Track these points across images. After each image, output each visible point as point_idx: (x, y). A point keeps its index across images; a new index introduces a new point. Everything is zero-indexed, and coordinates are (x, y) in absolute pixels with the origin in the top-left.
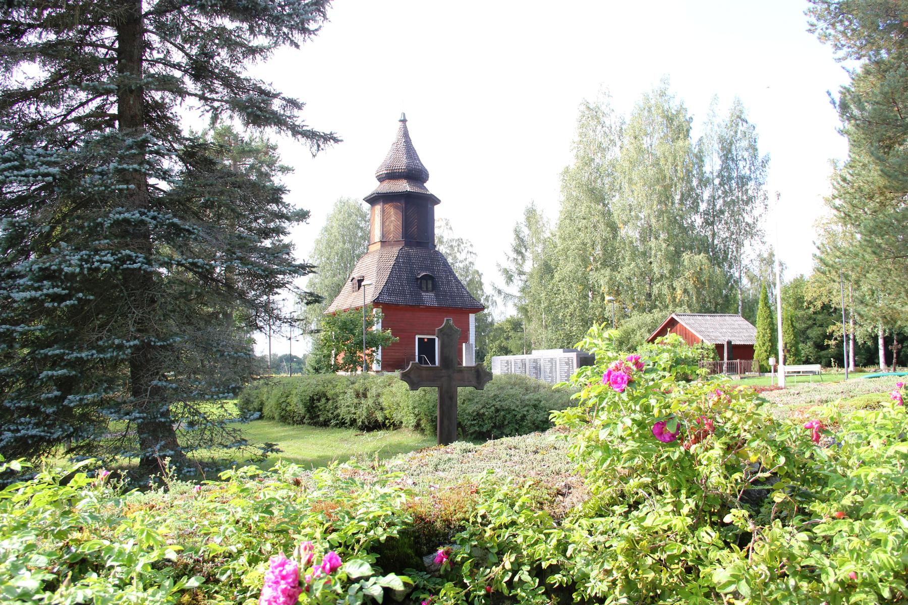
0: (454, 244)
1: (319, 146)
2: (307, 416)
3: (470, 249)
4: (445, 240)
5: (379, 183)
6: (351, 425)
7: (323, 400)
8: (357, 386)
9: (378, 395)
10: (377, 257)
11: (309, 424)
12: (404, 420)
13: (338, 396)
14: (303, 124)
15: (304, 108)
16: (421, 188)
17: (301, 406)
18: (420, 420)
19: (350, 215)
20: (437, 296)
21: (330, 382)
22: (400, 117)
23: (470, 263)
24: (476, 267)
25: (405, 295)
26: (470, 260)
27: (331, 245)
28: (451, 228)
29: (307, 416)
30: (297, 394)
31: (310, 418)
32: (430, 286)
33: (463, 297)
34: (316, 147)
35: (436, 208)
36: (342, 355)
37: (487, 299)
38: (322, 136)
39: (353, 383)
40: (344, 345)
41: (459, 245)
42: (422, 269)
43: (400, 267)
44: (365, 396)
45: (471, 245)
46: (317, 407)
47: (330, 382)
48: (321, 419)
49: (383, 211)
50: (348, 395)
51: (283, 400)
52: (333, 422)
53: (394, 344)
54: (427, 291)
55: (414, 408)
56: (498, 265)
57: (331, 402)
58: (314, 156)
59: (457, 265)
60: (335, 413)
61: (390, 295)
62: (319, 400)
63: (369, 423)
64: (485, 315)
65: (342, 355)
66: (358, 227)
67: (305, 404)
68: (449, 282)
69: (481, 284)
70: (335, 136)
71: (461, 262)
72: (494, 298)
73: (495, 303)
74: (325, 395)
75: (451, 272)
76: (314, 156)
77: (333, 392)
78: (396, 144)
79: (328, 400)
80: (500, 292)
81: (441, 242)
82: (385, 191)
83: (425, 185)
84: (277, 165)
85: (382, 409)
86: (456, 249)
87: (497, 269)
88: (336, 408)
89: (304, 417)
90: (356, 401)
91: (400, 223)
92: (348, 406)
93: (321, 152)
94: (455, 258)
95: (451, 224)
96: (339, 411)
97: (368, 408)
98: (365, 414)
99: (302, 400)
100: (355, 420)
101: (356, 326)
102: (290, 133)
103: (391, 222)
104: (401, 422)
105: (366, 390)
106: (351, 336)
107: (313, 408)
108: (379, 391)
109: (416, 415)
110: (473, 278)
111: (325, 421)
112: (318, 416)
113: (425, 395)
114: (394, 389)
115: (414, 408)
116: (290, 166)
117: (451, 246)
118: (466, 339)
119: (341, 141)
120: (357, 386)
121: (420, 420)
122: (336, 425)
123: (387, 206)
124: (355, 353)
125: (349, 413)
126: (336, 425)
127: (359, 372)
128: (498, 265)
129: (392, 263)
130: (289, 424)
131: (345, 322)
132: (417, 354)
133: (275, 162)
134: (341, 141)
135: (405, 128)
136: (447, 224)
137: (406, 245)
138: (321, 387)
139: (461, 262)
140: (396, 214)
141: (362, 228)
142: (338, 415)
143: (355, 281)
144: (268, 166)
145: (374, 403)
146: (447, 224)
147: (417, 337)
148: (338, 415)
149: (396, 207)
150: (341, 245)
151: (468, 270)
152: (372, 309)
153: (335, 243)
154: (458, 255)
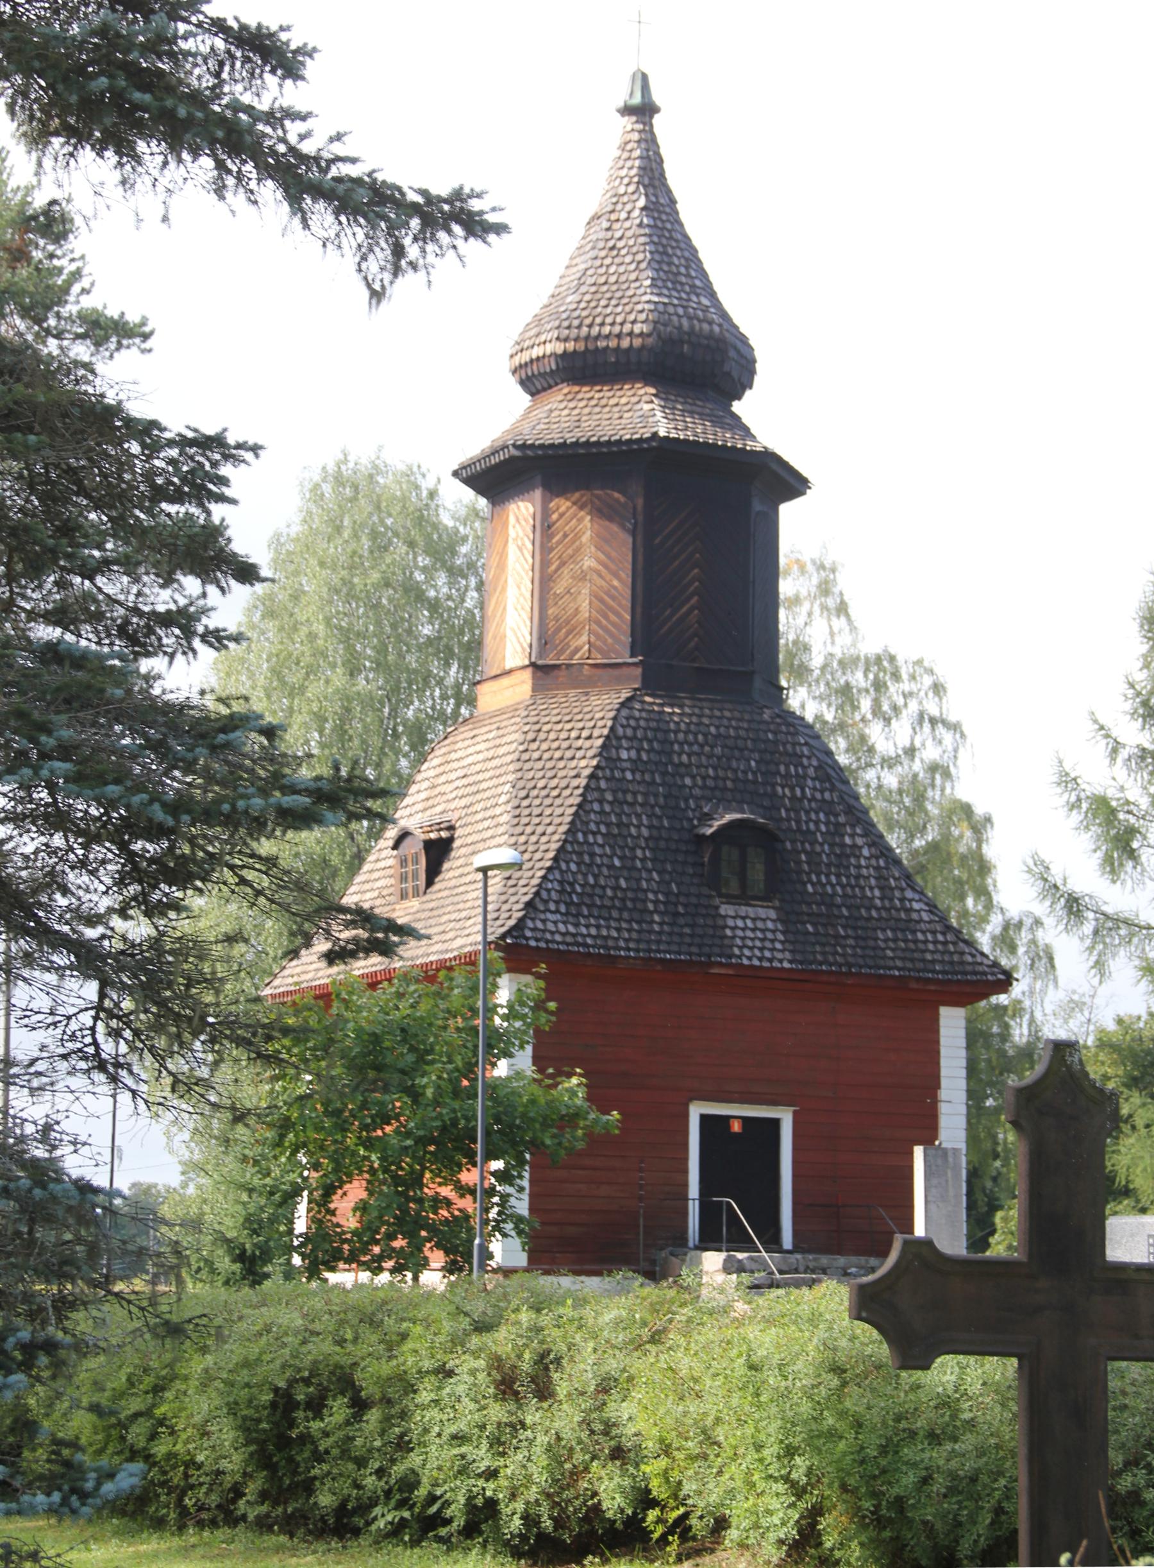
0: (858, 679)
1: (398, 251)
2: (252, 1489)
3: (933, 709)
4: (816, 661)
5: (524, 399)
6: (470, 1530)
7: (338, 1410)
8: (502, 1341)
9: (605, 1387)
10: (514, 737)
11: (263, 1525)
12: (739, 1513)
13: (411, 1389)
14: (338, 149)
15: (311, 68)
16: (717, 422)
17: (226, 1434)
18: (816, 1512)
19: (381, 547)
20: (788, 919)
21: (372, 1322)
22: (622, 92)
23: (933, 768)
24: (964, 789)
25: (641, 914)
26: (930, 753)
27: (293, 679)
28: (842, 609)
29: (252, 1489)
30: (207, 1379)
31: (263, 1496)
32: (757, 872)
33: (908, 925)
34: (383, 253)
35: (788, 512)
36: (356, 1191)
37: (1006, 940)
38: (415, 208)
39: (482, 1327)
40: (369, 1144)
41: (879, 686)
42: (725, 798)
43: (619, 786)
44: (544, 1392)
45: (938, 689)
46: (305, 1439)
47: (372, 1322)
48: (325, 1500)
49: (545, 529)
50: (459, 1386)
51: (135, 1405)
52: (384, 1517)
53: (598, 1141)
54: (743, 898)
55: (790, 1452)
56: (1067, 781)
57: (373, 1416)
58: (377, 295)
59: (870, 775)
60: (398, 1470)
61: (573, 914)
62: (317, 1407)
63: (559, 1523)
64: (1001, 1010)
65: (356, 1191)
66: (415, 594)
67: (247, 1427)
68: (844, 856)
69: (984, 868)
70: (475, 205)
71: (889, 763)
72: (1045, 936)
73: (1044, 960)
74: (345, 1382)
75: (857, 814)
76: (377, 295)
77: (386, 1368)
78: (605, 218)
79: (360, 1405)
80: (1074, 906)
81: (801, 673)
82: (554, 437)
83: (737, 407)
84: (70, 309)
85: (618, 1453)
86: (866, 704)
87: (1059, 798)
88: (403, 1445)
89: (237, 1492)
90: (497, 1412)
91: (621, 585)
92: (459, 1438)
93: (409, 281)
94: (862, 746)
95: (844, 583)
96: (415, 1459)
97: (557, 1451)
98: (541, 1478)
99: (232, 1409)
100: (492, 1504)
101: (422, 1056)
102: (269, 192)
103: (582, 577)
104: (721, 1524)
105: (546, 1362)
106: (399, 1102)
107: (283, 1442)
108: (612, 1365)
109: (799, 1492)
110: (947, 837)
111: (341, 1510)
112: (308, 1487)
113: (839, 1393)
114: (685, 1364)
115: (790, 1452)
116: (133, 318)
117: (846, 691)
118: (928, 1132)
119: (500, 229)
120: (502, 1341)
121: (816, 1512)
122: (396, 1531)
123: (562, 504)
124: (418, 1182)
125: (463, 1471)
126: (396, 1531)
127: (433, 1279)
128: (1067, 781)
129: (586, 765)
130: (159, 1524)
131: (376, 1039)
132: (694, 1191)
133: (60, 295)
134: (500, 229)
135: (649, 141)
136: (825, 589)
137: (650, 684)
138: (327, 1347)
139: (889, 763)
140: (601, 541)
141: (434, 606)
142: (410, 1483)
143: (414, 847)
144: (25, 312)
145: (586, 1423)
146: (825, 589)
147: (696, 1111)
148: (410, 1483)
149: (603, 512)
150: (338, 678)
151: (920, 799)
152: (492, 974)
153: (311, 671)
154: (875, 732)
